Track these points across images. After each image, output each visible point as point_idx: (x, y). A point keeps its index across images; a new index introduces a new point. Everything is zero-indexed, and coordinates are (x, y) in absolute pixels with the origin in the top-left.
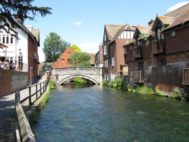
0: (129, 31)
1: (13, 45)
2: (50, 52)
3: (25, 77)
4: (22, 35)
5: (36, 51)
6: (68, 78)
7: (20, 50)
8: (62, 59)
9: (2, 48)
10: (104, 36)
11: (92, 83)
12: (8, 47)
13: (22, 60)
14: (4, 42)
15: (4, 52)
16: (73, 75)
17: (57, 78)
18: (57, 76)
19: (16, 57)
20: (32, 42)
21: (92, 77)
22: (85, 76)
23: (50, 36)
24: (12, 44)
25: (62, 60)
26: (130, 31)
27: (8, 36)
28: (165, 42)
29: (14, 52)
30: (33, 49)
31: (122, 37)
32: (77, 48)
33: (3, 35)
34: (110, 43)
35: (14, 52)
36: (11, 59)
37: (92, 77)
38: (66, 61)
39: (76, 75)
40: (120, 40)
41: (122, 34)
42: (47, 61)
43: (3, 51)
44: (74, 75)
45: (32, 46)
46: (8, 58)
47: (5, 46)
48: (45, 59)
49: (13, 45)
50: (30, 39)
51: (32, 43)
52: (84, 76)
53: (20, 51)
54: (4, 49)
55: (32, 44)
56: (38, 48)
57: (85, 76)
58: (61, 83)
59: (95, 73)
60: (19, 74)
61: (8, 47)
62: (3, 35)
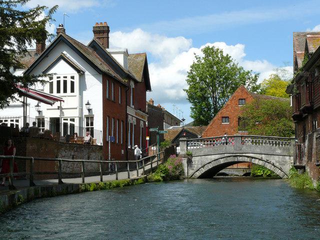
1: (75, 96)
2: (204, 98)
4: (93, 75)
6: (272, 168)
7: (88, 104)
8: (223, 117)
12: (64, 101)
13: (92, 124)
15: (58, 109)
16: (226, 155)
17: (190, 162)
18: (189, 157)
19: (81, 119)
21: (274, 159)
22: (255, 158)
23: (204, 56)
24: (72, 94)
25: (224, 119)
27: (65, 79)
29: (76, 108)
34: (64, 132)
35: (76, 108)
36: (72, 123)
37: (274, 159)
38: (235, 122)
39: (234, 156)
42: (194, 124)
44: (229, 155)
46: (67, 120)
47: (56, 100)
48: (192, 117)
49: (75, 96)
52: (253, 158)
53: (88, 106)
54: (57, 104)
56: (148, 93)
57: (255, 158)
58: (198, 174)
59: (279, 151)
61: (64, 101)
62: (58, 78)
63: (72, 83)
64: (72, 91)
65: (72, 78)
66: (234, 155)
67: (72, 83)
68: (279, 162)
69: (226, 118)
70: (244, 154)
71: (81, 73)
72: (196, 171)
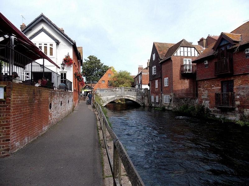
0: (182, 47)
26: (187, 47)
31: (179, 55)
63: (51, 49)
65: (51, 45)
67: (51, 49)
68: (140, 99)
71: (58, 43)
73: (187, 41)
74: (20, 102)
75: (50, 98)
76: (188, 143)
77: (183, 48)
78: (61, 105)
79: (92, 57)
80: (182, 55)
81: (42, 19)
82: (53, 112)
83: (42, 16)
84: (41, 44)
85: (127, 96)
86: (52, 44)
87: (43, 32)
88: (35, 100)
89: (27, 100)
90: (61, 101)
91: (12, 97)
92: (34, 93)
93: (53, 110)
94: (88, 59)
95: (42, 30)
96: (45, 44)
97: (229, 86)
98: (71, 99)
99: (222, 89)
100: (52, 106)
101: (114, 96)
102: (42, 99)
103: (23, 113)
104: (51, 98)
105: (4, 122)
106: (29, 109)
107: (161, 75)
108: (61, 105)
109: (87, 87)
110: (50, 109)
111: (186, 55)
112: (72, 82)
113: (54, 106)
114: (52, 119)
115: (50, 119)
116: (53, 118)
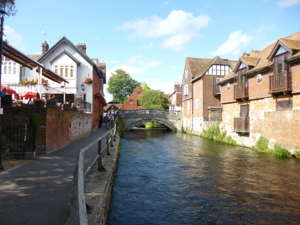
0: (219, 65)
3: (89, 120)
5: (101, 88)
9: (60, 83)
10: (184, 72)
11: (165, 128)
12: (68, 83)
14: (66, 76)
20: (97, 76)
26: (221, 65)
27: (67, 68)
28: (234, 88)
30: (99, 86)
31: (210, 73)
32: (104, 96)
33: (66, 66)
40: (208, 77)
41: (210, 70)
43: (61, 87)
45: (97, 81)
50: (96, 72)
51: (97, 78)
53: (83, 87)
55: (97, 80)
60: (81, 117)
61: (68, 83)
64: (72, 76)
65: (72, 67)
66: (149, 118)
69: (131, 100)
70: (154, 118)
72: (130, 126)
73: (220, 58)
74: (51, 121)
75: (70, 119)
76: (254, 181)
77: (220, 66)
78: (79, 126)
79: (120, 71)
80: (214, 74)
81: (64, 42)
82: (72, 130)
83: (64, 38)
84: (63, 66)
85: (156, 118)
86: (73, 66)
87: (65, 55)
88: (59, 120)
89: (54, 120)
90: (79, 121)
91: (47, 117)
92: (59, 115)
93: (72, 129)
94: (116, 73)
95: (65, 53)
96: (66, 66)
97: (245, 110)
98: (288, 118)
99: (241, 114)
100: (72, 126)
101: (141, 119)
102: (64, 120)
103: (53, 128)
104: (71, 119)
105: (43, 132)
106: (56, 126)
107: (193, 96)
108: (79, 126)
109: (112, 107)
110: (70, 127)
111: (219, 74)
112: (92, 103)
113: (73, 125)
114: (71, 137)
115: (70, 136)
116: (73, 136)
